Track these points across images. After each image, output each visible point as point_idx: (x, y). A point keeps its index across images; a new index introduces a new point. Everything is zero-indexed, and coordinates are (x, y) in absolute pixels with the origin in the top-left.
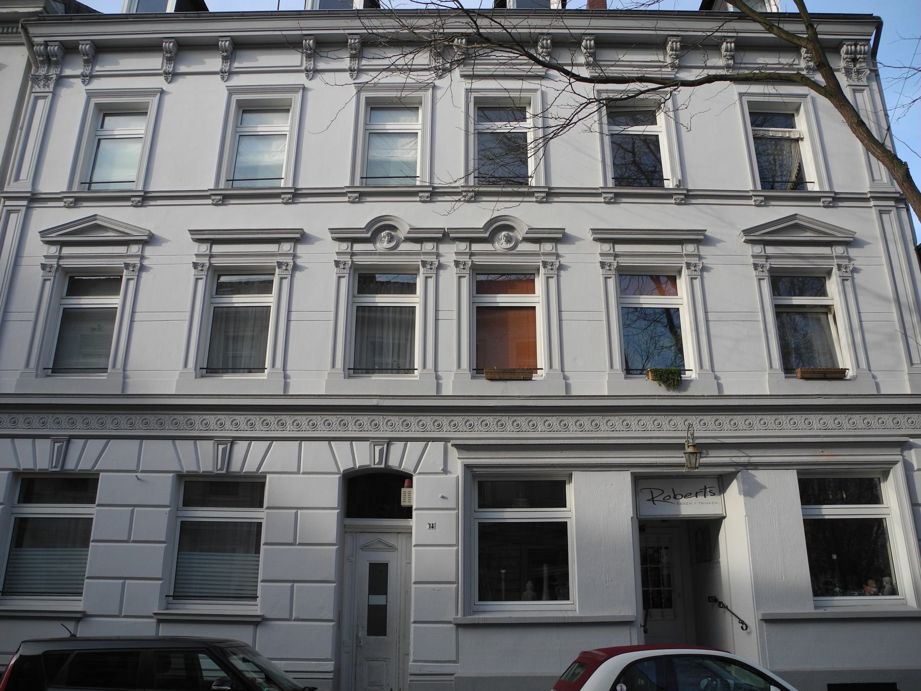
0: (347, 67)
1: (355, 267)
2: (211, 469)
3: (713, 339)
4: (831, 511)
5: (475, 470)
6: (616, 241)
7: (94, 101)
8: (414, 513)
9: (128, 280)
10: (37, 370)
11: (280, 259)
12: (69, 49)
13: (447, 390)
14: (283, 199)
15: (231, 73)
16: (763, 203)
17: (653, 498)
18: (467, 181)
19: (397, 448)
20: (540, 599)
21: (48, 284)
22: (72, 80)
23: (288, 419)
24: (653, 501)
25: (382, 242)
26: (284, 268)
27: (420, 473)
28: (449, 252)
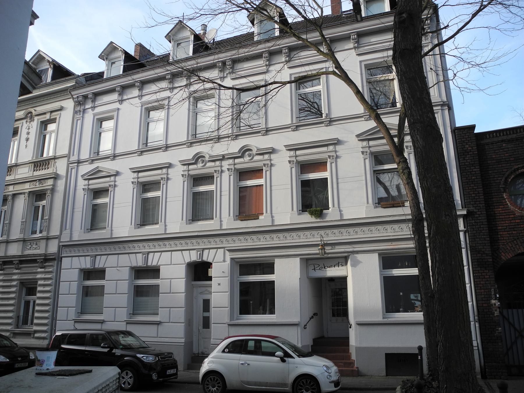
0: (137, 95)
1: (372, 153)
2: (141, 265)
3: (340, 191)
4: (397, 272)
5: (236, 260)
6: (296, 150)
7: (96, 117)
8: (213, 279)
9: (217, 177)
10: (234, 217)
11: (216, 169)
12: (85, 97)
13: (224, 227)
14: (262, 133)
15: (142, 96)
16: (369, 119)
17: (315, 268)
18: (233, 130)
19: (206, 252)
20: (265, 314)
21: (86, 196)
22: (88, 110)
23: (167, 243)
24: (315, 270)
25: (199, 163)
26: (332, 158)
27: (215, 262)
28: (226, 164)
